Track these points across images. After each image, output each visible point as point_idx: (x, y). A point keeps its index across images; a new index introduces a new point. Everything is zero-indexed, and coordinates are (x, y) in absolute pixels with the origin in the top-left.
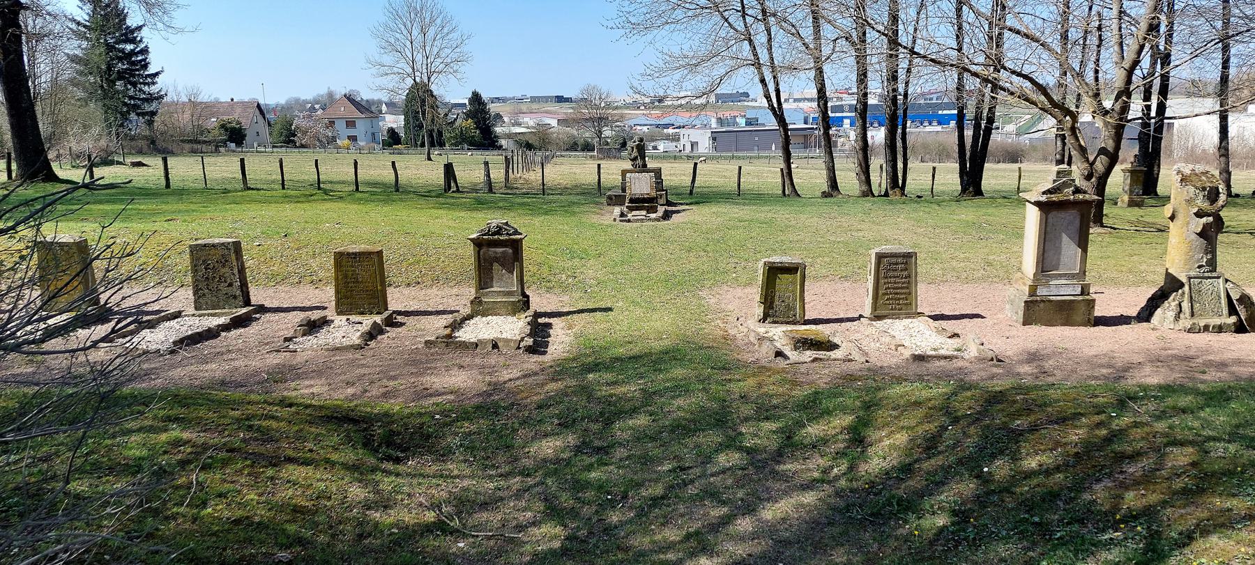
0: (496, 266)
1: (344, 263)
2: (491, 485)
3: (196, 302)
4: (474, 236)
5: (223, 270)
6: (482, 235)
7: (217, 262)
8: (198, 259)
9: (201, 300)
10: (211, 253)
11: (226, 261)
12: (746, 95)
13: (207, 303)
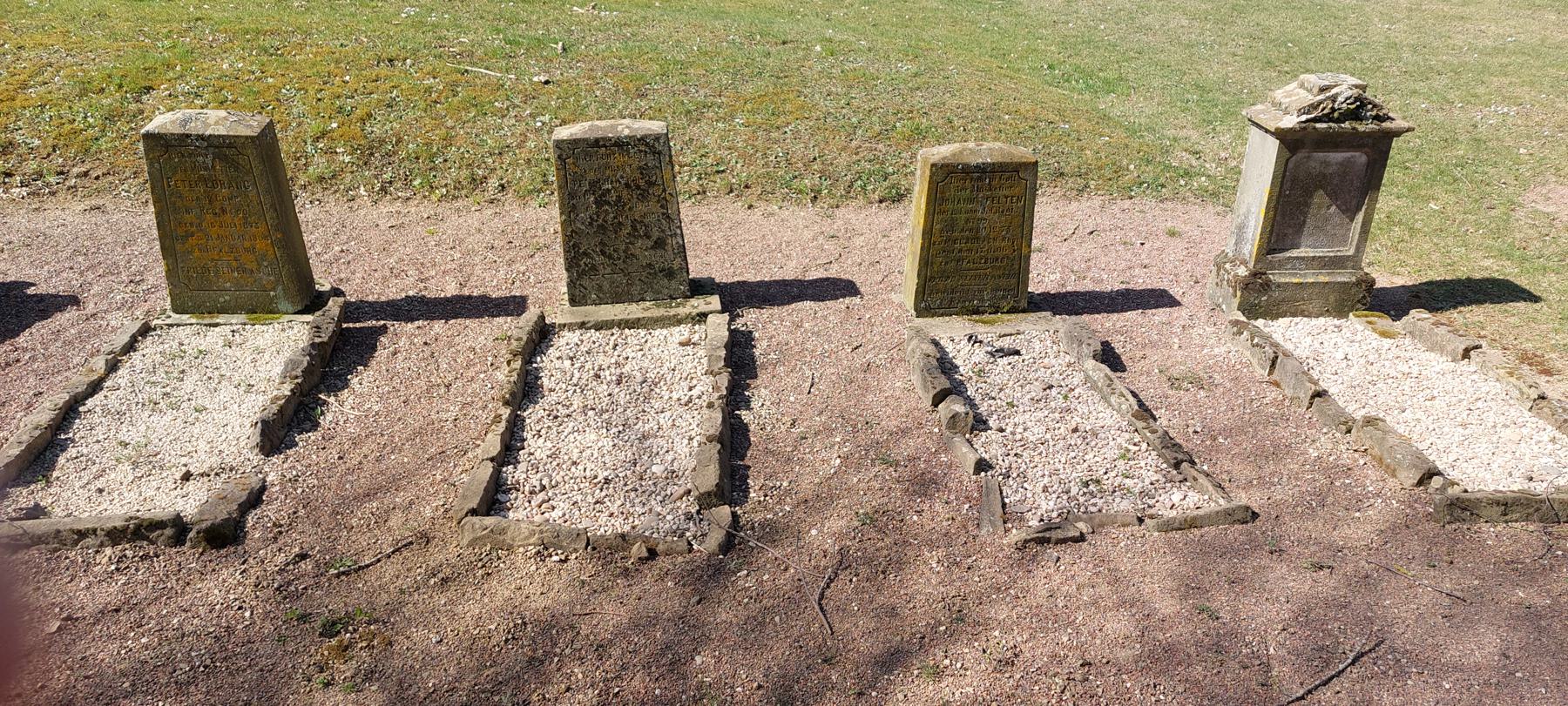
0: (1319, 198)
1: (949, 194)
2: (114, 588)
3: (571, 284)
4: (1290, 122)
5: (641, 208)
6: (1315, 120)
7: (627, 185)
8: (578, 179)
9: (586, 282)
10: (611, 161)
11: (651, 184)
13: (600, 288)
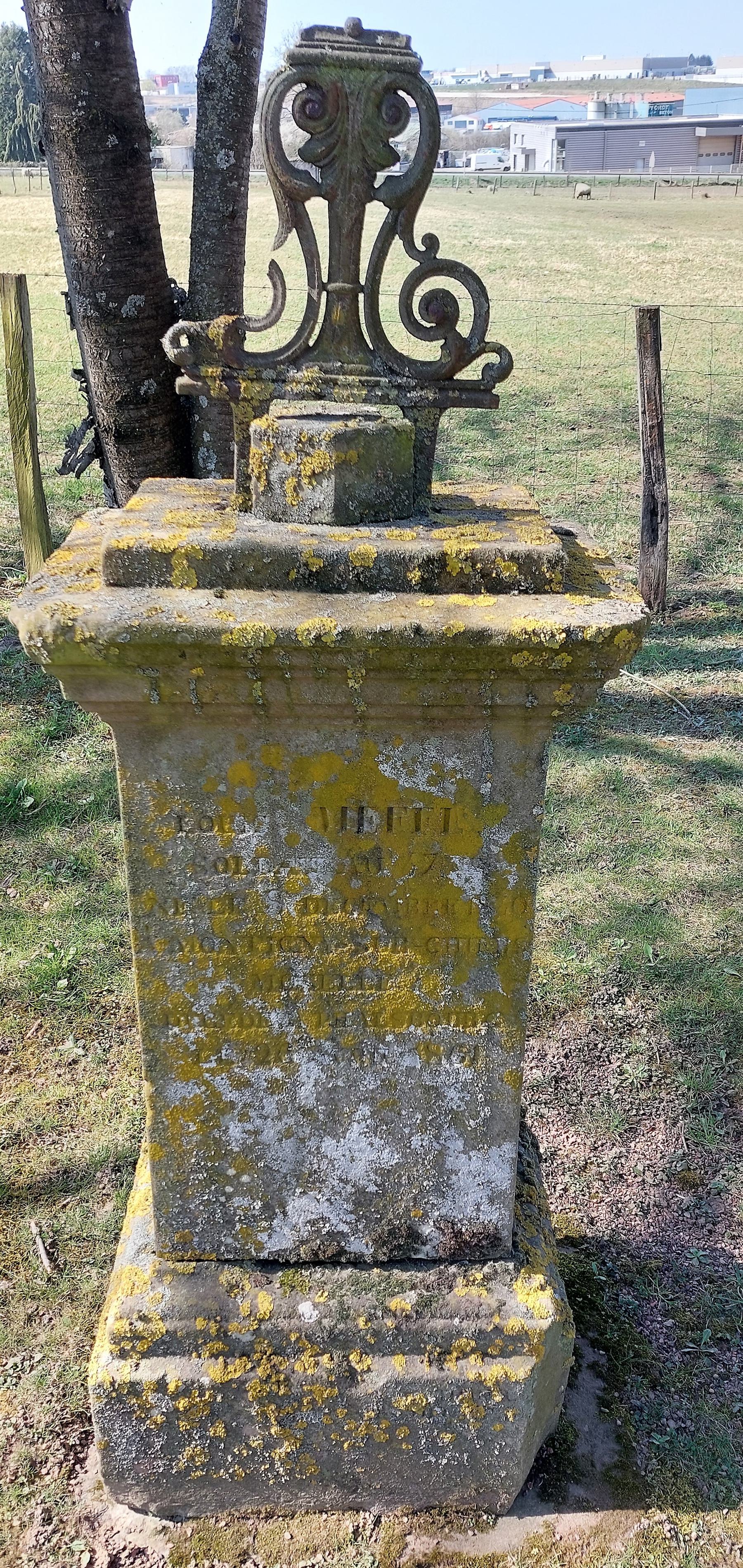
12: (706, 61)
